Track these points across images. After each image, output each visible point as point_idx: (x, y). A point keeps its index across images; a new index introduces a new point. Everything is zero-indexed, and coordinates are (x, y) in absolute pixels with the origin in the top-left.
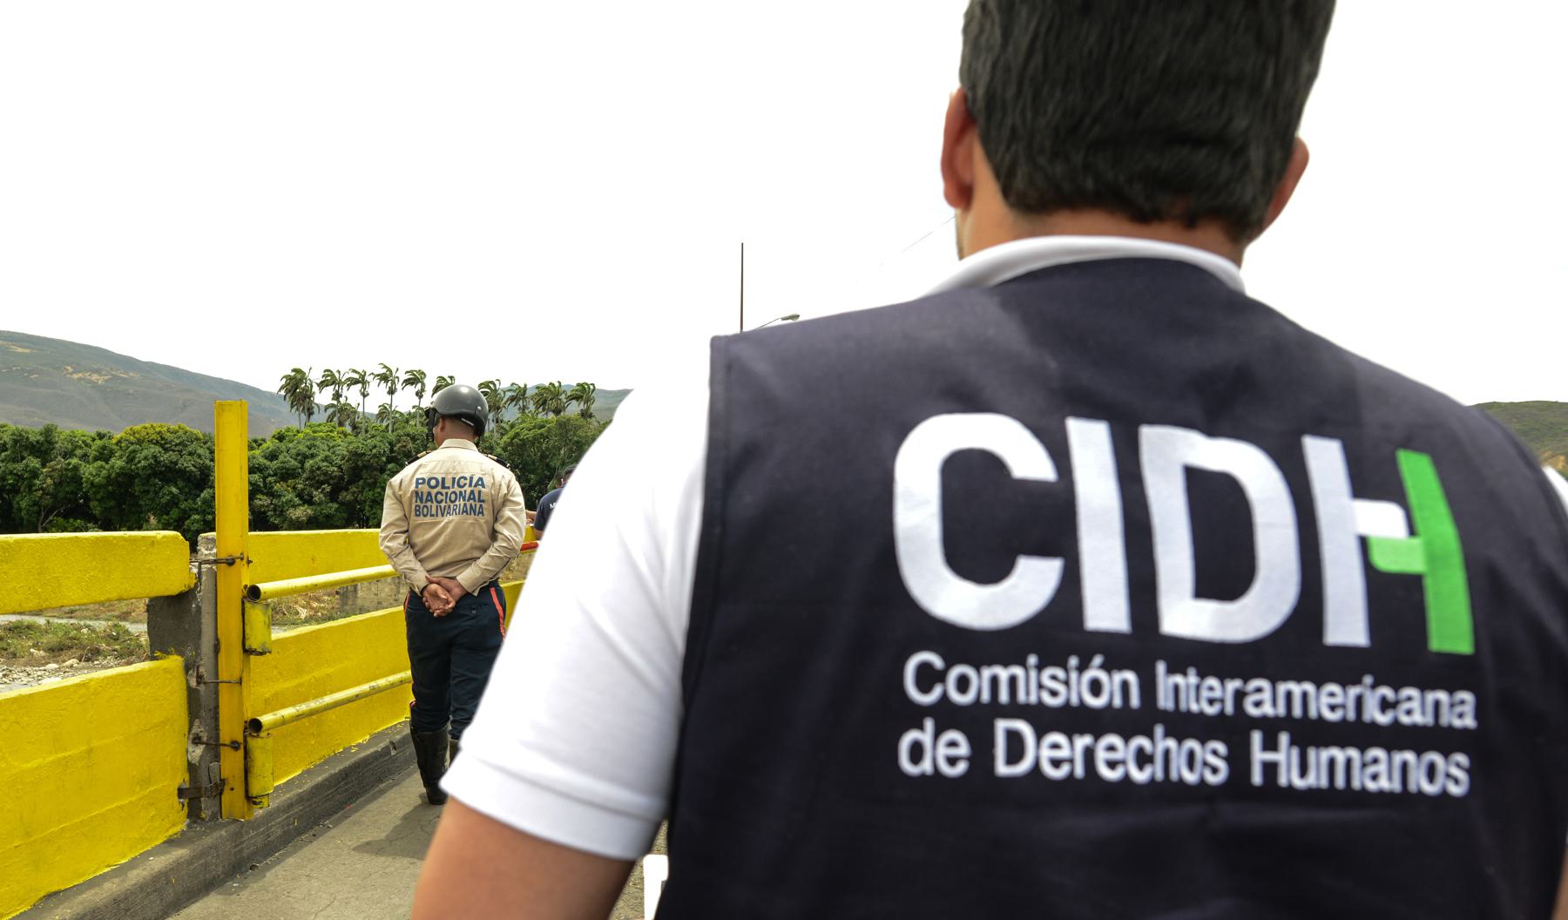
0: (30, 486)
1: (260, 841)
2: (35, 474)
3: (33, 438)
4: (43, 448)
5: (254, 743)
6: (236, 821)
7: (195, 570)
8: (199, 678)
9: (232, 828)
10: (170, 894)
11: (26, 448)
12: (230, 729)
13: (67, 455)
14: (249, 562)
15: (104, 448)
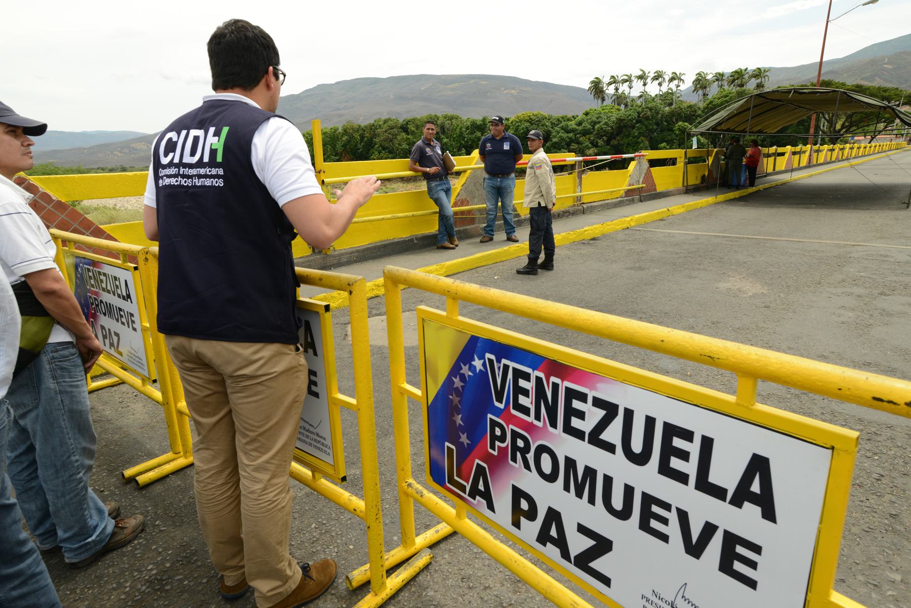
1: (336, 262)
3: (478, 123)
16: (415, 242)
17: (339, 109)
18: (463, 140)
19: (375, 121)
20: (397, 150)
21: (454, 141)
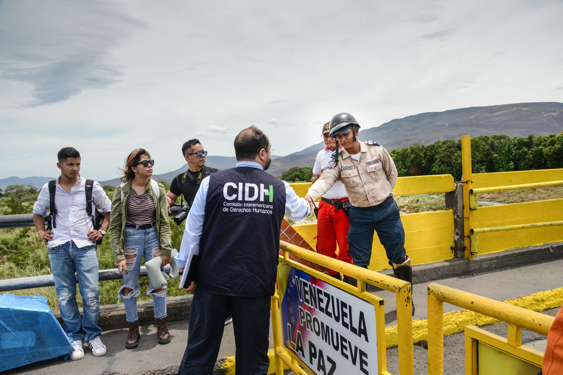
0: (524, 158)
1: (477, 267)
2: (526, 153)
3: (525, 141)
4: (529, 143)
5: (472, 236)
6: (468, 259)
7: (456, 185)
8: (458, 216)
9: (465, 261)
10: (440, 274)
11: (523, 144)
12: (466, 233)
13: (538, 145)
14: (472, 182)
15: (552, 141)
16: (551, 251)
17: (406, 136)
18: (511, 154)
19: (435, 143)
20: (454, 164)
21: (503, 155)
